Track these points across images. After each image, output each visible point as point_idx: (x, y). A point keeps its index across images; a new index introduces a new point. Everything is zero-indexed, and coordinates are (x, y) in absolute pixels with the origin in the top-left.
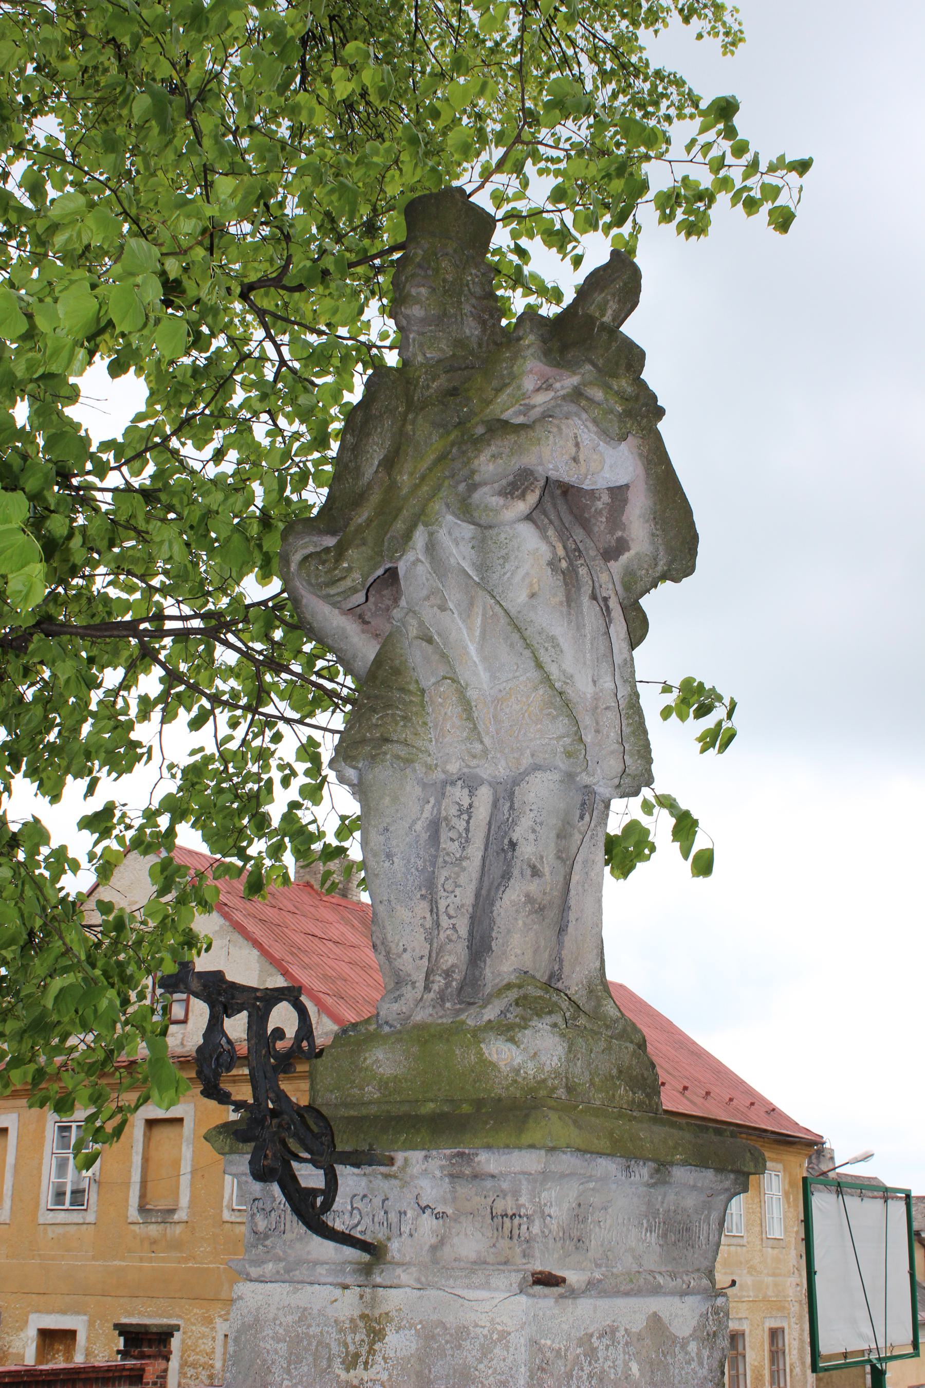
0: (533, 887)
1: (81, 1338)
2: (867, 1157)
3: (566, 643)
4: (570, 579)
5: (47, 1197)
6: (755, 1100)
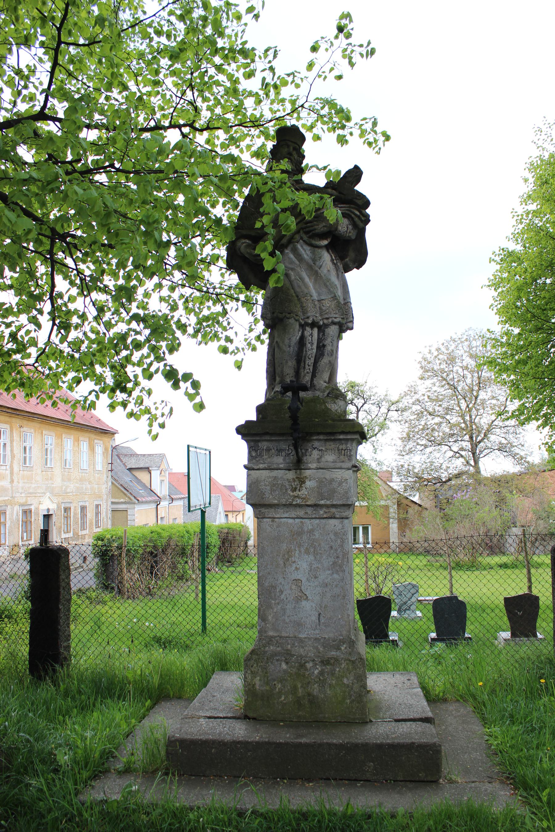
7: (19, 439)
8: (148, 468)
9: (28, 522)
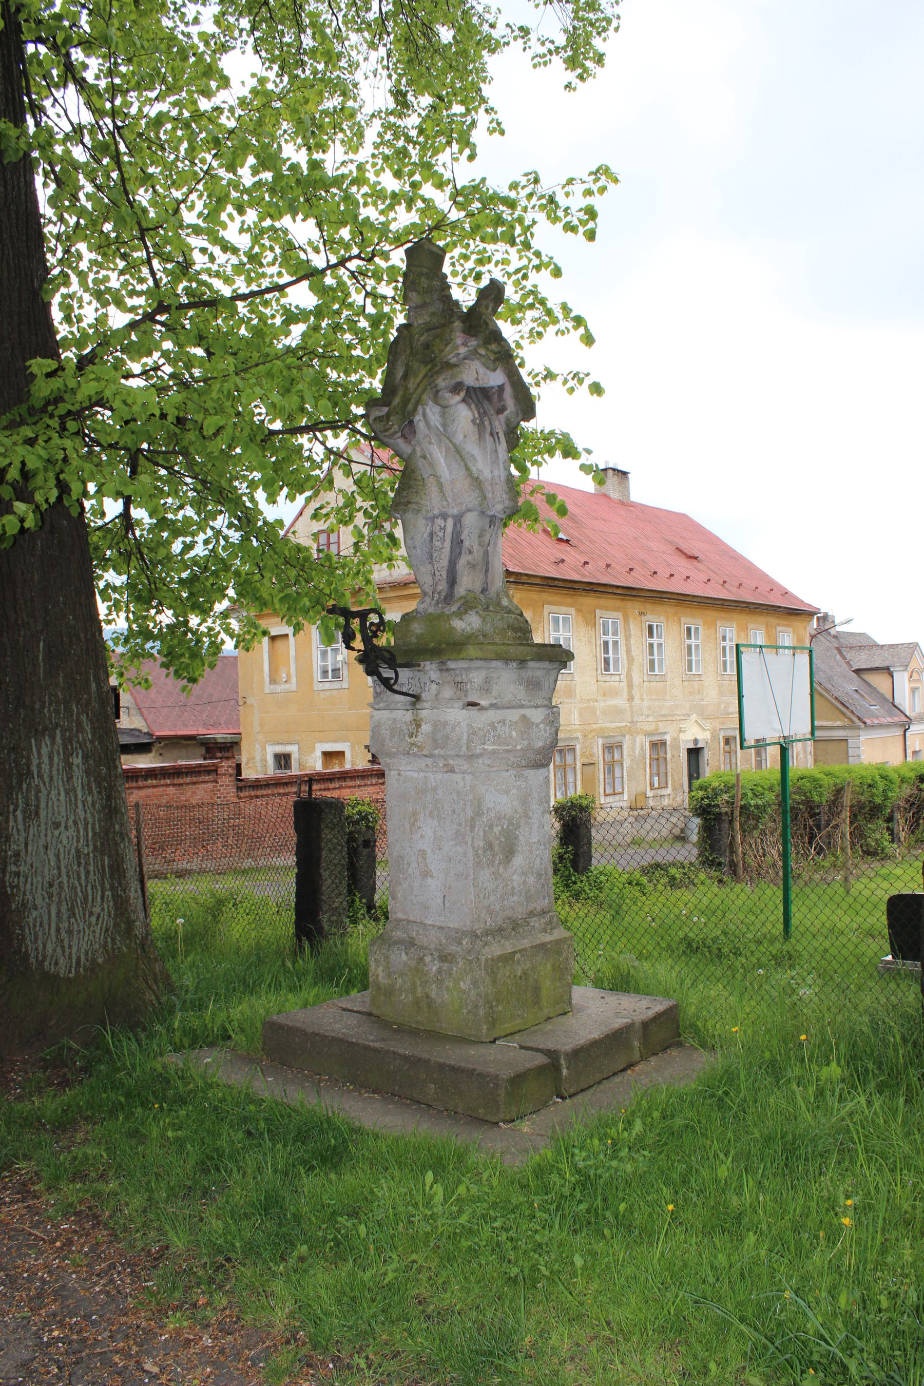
0: (470, 558)
1: (348, 755)
2: (848, 622)
3: (479, 457)
4: (480, 427)
5: (317, 675)
6: (773, 587)
7: (639, 634)
8: (888, 668)
9: (661, 761)
